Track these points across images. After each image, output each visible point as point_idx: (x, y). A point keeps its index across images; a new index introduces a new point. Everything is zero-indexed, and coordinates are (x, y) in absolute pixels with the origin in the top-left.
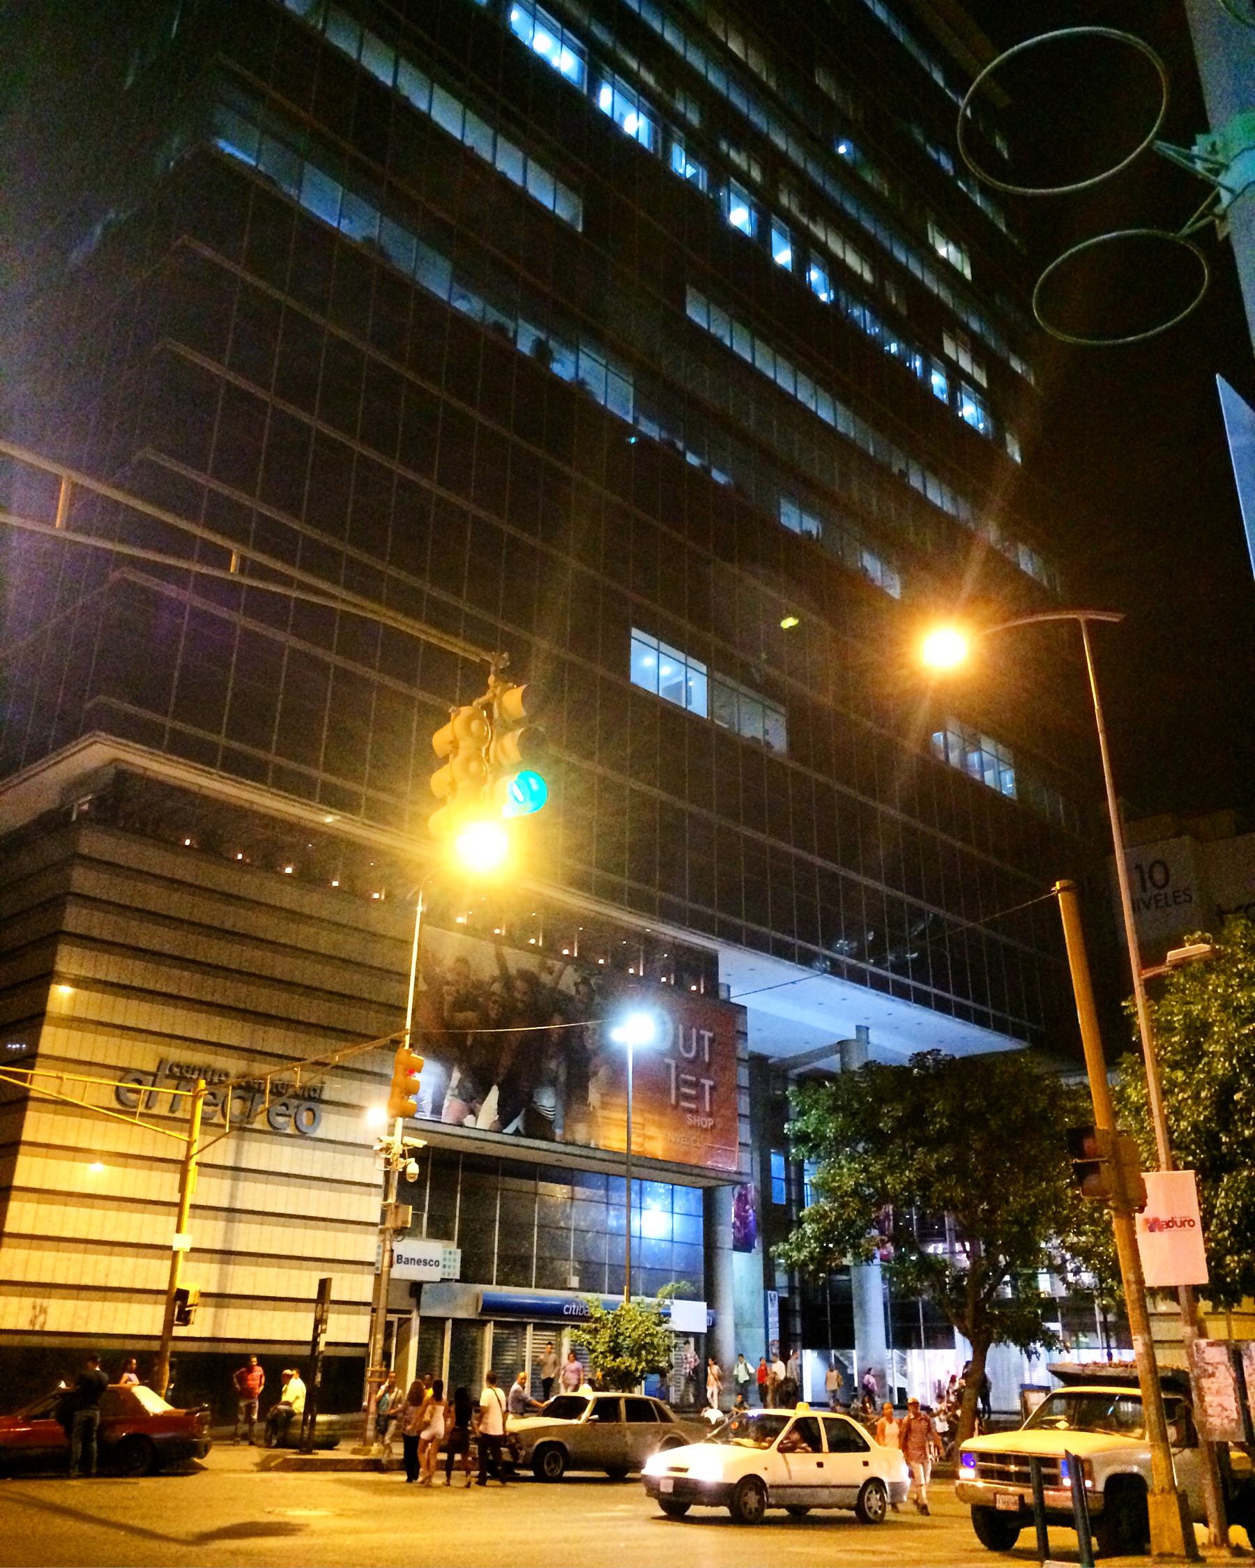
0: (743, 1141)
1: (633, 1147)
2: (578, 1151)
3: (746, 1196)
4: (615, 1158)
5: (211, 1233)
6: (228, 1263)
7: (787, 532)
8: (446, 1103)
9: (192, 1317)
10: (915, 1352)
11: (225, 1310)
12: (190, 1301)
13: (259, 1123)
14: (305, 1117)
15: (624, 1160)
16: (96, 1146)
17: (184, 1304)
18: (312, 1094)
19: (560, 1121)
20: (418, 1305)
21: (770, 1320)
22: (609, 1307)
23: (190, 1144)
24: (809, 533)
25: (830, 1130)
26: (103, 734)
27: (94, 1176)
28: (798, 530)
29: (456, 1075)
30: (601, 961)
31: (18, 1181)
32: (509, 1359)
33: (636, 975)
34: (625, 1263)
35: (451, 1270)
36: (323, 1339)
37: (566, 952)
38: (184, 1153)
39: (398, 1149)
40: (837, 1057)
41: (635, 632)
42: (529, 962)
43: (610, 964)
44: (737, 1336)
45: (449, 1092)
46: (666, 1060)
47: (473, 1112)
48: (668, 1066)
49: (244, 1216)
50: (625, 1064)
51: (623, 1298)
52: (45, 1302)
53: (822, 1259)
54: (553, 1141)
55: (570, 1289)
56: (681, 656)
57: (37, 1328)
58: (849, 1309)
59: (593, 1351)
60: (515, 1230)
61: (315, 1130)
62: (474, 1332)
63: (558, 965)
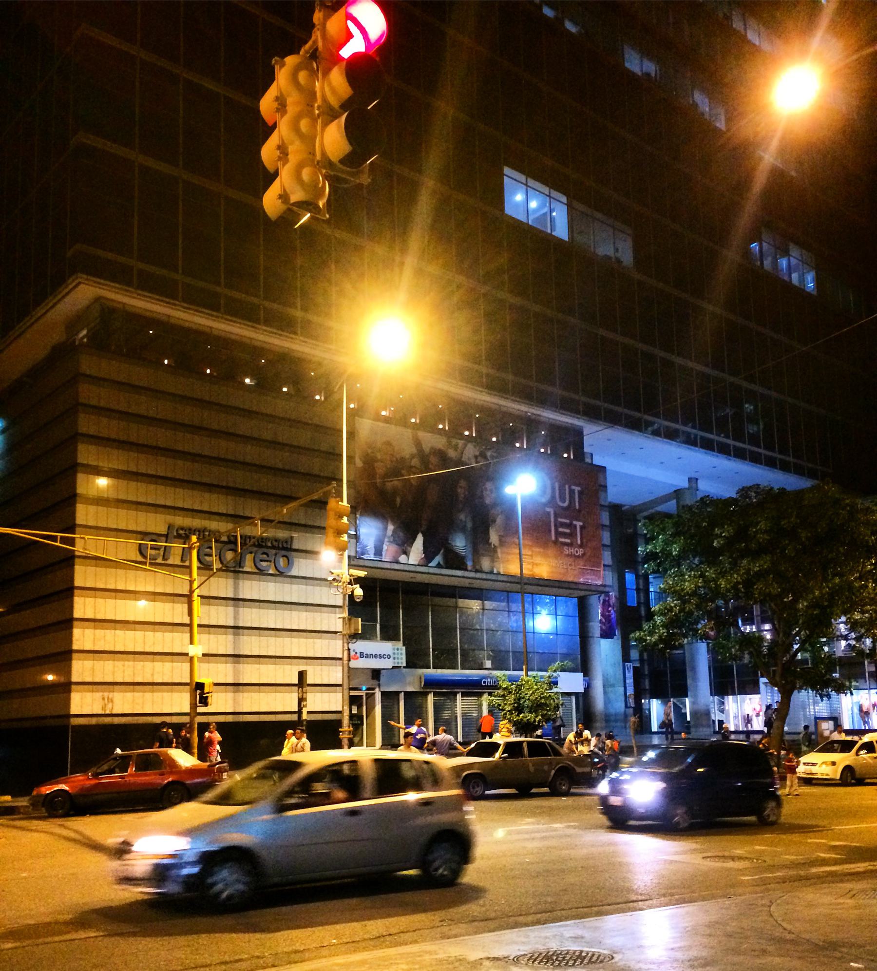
0: (606, 563)
1: (524, 571)
2: (484, 576)
3: (608, 601)
4: (512, 579)
5: (223, 643)
6: (239, 663)
7: (631, 75)
8: (385, 547)
9: (209, 700)
10: (731, 697)
11: (241, 694)
12: (206, 690)
13: (248, 566)
14: (282, 562)
15: (519, 581)
16: (140, 588)
17: (202, 693)
18: (285, 545)
19: (470, 556)
20: (379, 686)
21: (627, 681)
22: (512, 680)
23: (191, 582)
24: (648, 75)
25: (675, 550)
26: (85, 276)
27: (142, 609)
28: (640, 74)
29: (391, 527)
30: (494, 439)
31: (76, 615)
32: (446, 715)
33: (521, 448)
34: (524, 650)
35: (400, 661)
36: (305, 711)
37: (467, 433)
38: (188, 588)
39: (346, 578)
40: (674, 501)
41: (507, 170)
42: (440, 442)
43: (503, 437)
44: (605, 693)
45: (386, 540)
46: (548, 509)
47: (406, 553)
48: (549, 513)
49: (246, 631)
50: (515, 506)
51: (523, 673)
52: (111, 695)
53: (669, 642)
54: (466, 570)
55: (486, 669)
56: (546, 190)
57: (108, 712)
58: (684, 672)
59: (503, 710)
60: (444, 632)
61: (290, 571)
62: (419, 700)
63: (461, 443)
